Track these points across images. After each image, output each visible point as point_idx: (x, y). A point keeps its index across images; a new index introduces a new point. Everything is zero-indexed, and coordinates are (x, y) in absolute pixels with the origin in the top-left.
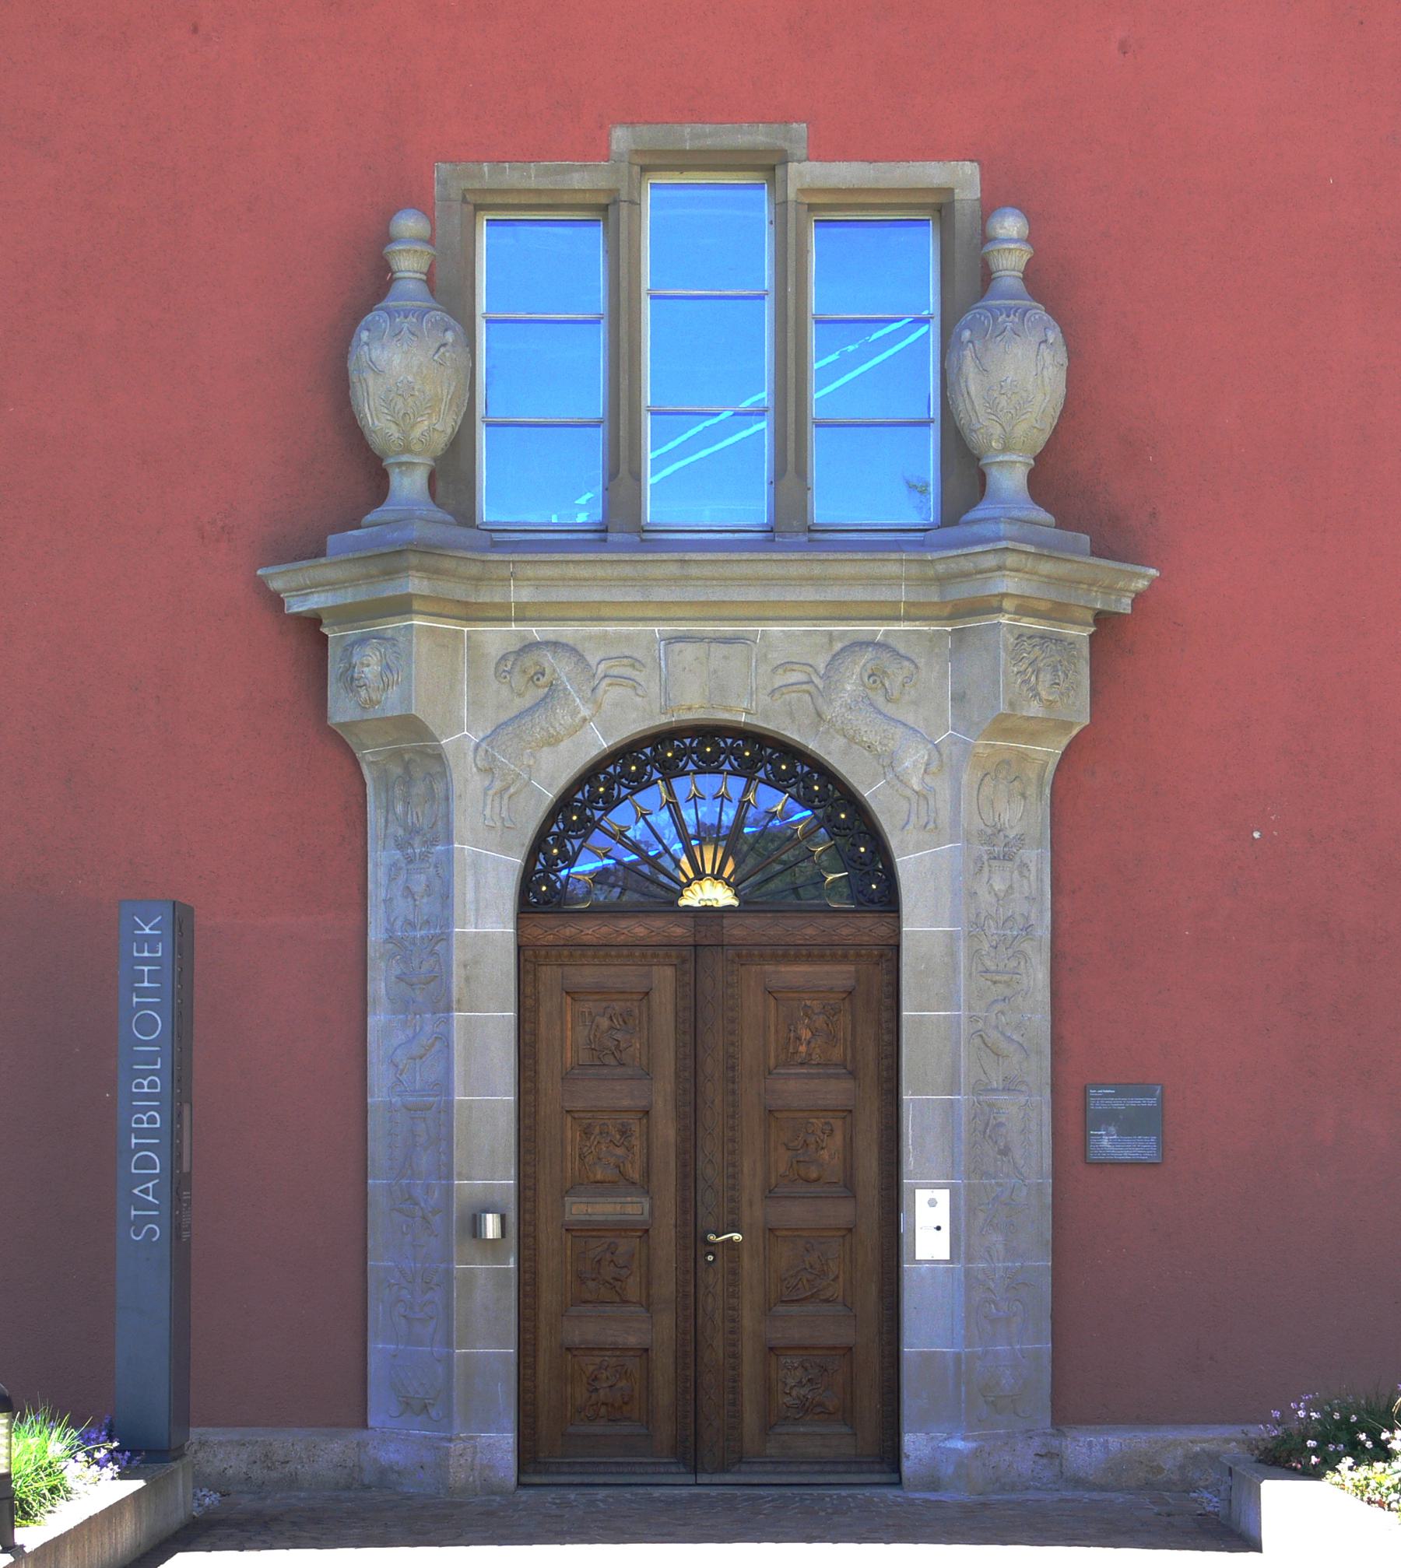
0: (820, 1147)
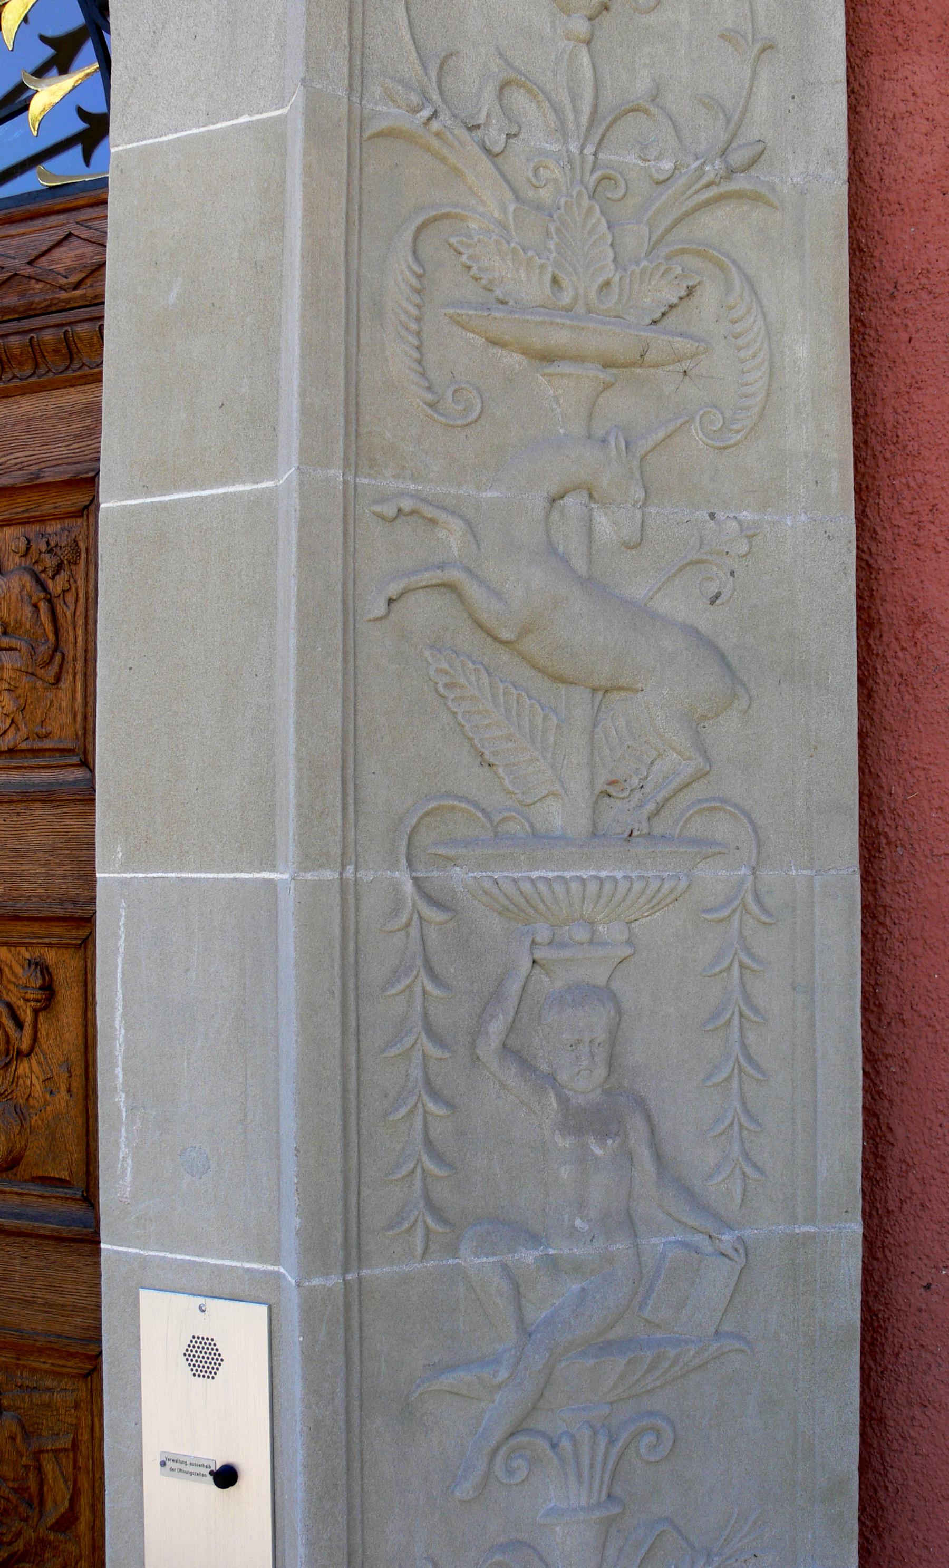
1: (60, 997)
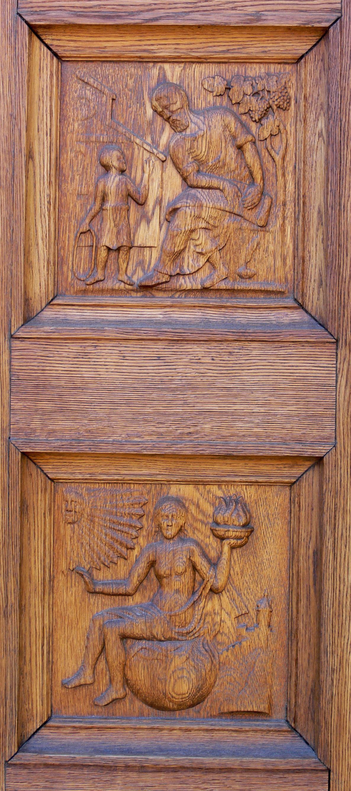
0: (202, 589)
1: (258, 533)
